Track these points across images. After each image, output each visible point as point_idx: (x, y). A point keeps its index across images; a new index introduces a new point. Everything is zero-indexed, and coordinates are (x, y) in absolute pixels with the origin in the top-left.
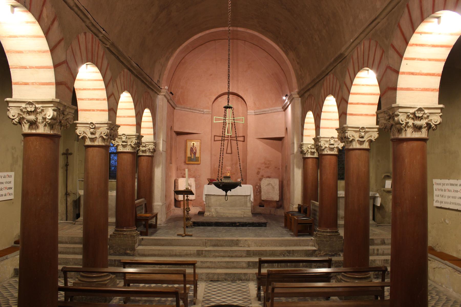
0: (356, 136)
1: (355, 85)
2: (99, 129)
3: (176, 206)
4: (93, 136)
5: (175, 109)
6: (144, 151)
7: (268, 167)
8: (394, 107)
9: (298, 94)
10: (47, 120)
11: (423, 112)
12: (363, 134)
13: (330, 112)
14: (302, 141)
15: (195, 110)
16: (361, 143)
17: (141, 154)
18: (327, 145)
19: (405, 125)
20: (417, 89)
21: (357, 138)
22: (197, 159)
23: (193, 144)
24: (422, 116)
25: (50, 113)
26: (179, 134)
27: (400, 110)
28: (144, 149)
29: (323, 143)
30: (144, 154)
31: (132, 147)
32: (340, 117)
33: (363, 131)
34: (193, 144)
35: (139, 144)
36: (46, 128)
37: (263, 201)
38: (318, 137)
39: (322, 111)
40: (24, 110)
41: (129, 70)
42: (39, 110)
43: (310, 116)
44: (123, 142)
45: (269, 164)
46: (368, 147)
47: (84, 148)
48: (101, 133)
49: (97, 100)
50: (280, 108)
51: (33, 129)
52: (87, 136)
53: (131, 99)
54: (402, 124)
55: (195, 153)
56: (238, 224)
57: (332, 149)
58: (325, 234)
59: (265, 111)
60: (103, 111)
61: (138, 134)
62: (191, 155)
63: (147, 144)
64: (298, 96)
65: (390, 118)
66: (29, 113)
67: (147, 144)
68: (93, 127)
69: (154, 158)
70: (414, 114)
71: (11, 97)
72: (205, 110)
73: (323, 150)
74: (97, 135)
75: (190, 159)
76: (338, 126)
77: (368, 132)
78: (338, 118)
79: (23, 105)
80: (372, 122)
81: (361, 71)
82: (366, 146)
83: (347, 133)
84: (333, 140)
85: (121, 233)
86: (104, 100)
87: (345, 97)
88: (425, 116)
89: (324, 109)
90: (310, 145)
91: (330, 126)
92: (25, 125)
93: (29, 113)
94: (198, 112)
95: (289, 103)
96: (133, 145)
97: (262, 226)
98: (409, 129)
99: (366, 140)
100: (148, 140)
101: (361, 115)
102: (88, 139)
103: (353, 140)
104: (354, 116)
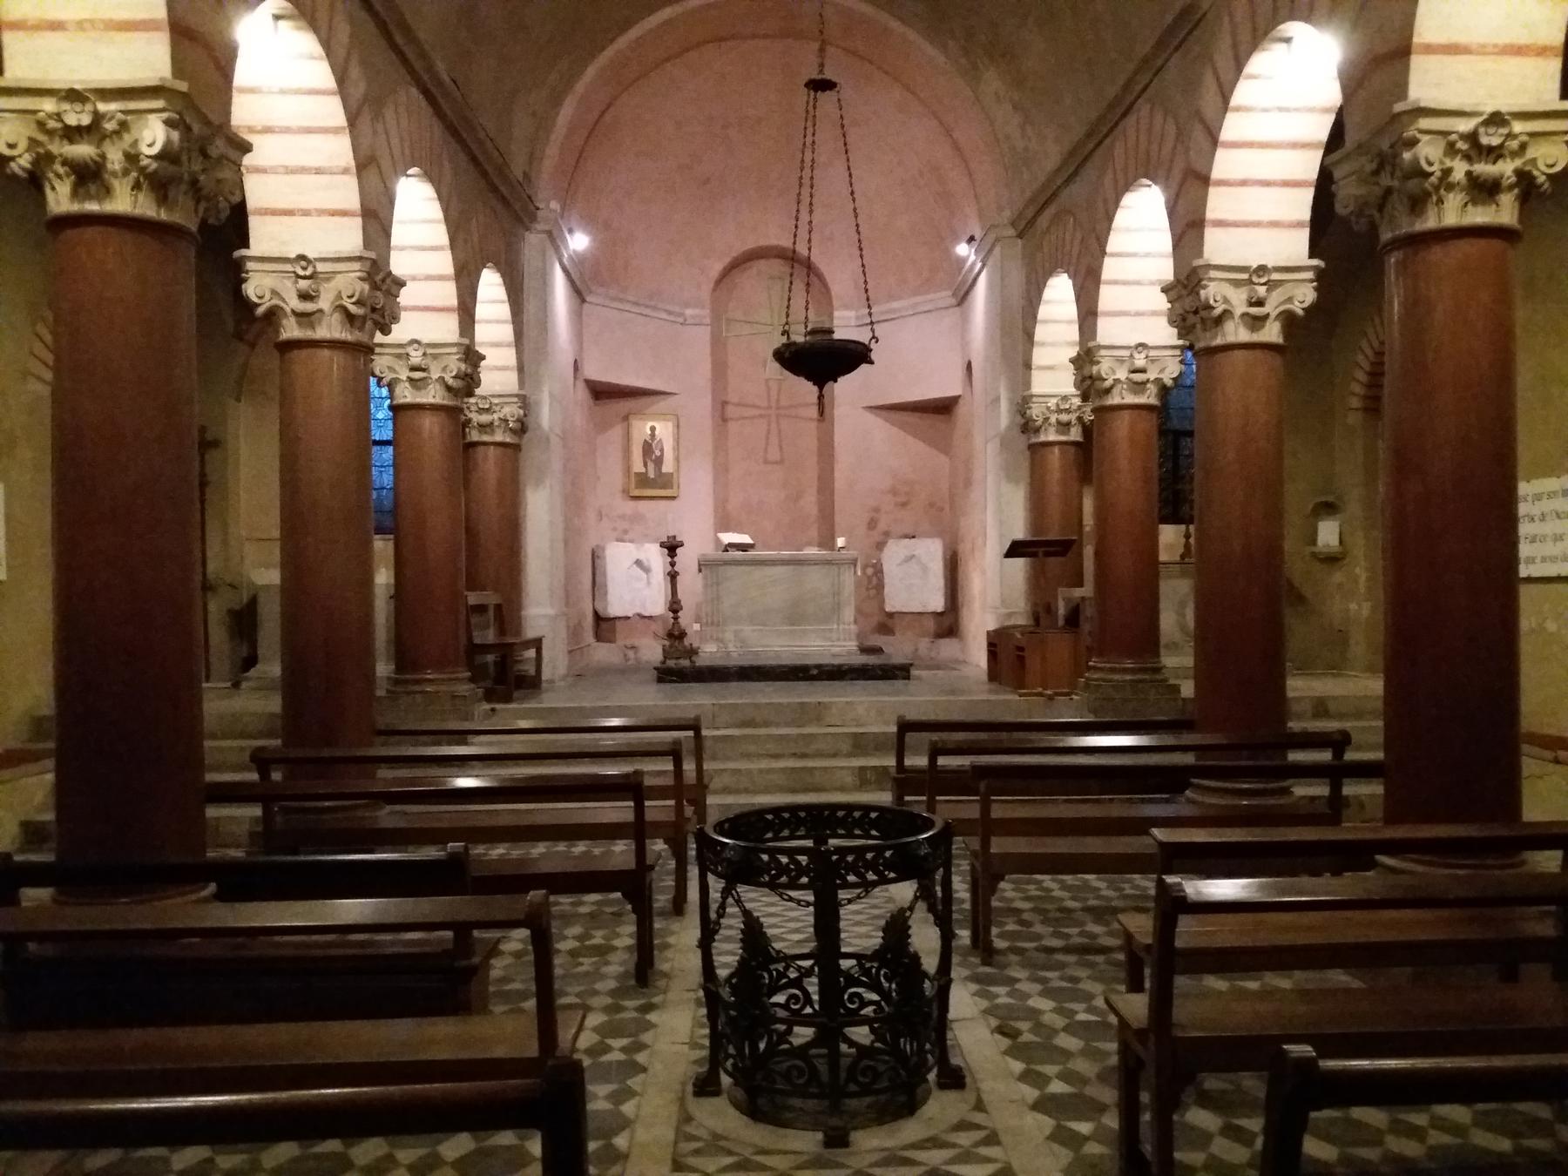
0: (1238, 300)
1: (1238, 109)
2: (328, 280)
3: (599, 637)
4: (309, 307)
5: (583, 301)
6: (486, 428)
7: (904, 505)
8: (1400, 114)
9: (1013, 224)
10: (145, 162)
11: (1504, 131)
12: (1262, 290)
13: (1134, 255)
14: (1027, 384)
15: (655, 308)
16: (1256, 322)
17: (475, 436)
18: (1122, 374)
19: (1441, 179)
20: (1482, 50)
21: (1240, 307)
22: (665, 481)
23: (653, 429)
24: (1501, 146)
25: (153, 135)
26: (602, 393)
27: (1425, 123)
28: (485, 418)
29: (1110, 370)
30: (486, 438)
31: (449, 388)
32: (1176, 246)
33: (1263, 280)
34: (653, 429)
35: (468, 382)
36: (141, 197)
37: (891, 615)
38: (1091, 344)
39: (1104, 253)
40: (52, 124)
41: (426, 93)
42: (110, 126)
43: (1060, 292)
44: (414, 369)
45: (907, 494)
46: (1280, 340)
47: (276, 354)
48: (339, 296)
49: (318, 171)
50: (944, 297)
51: (89, 197)
52: (288, 310)
53: (435, 210)
54: (1432, 174)
55: (659, 462)
56: (815, 672)
57: (1139, 387)
58: (1117, 677)
59: (894, 311)
60: (344, 213)
61: (466, 341)
62: (645, 465)
63: (496, 401)
64: (1011, 232)
65: (1381, 167)
66: (72, 134)
67: (496, 401)
68: (308, 273)
69: (523, 455)
70: (1472, 137)
71: (248, 247)
72: (689, 312)
73: (1108, 391)
74: (324, 303)
75: (643, 480)
76: (1169, 275)
77: (1281, 282)
78: (1170, 249)
79: (48, 105)
80: (1293, 247)
81: (1266, 44)
82: (1272, 333)
83: (1205, 287)
84: (1143, 355)
85: (417, 688)
86: (345, 171)
87: (1199, 166)
88: (1514, 144)
89: (1114, 243)
90: (1054, 401)
91: (1133, 308)
92: (57, 183)
93: (72, 134)
94: (664, 316)
95: (979, 265)
96: (451, 382)
97: (895, 677)
98: (1451, 195)
99: (1273, 314)
100: (498, 389)
101: (1257, 224)
102: (293, 319)
103: (1227, 314)
104: (1232, 230)
